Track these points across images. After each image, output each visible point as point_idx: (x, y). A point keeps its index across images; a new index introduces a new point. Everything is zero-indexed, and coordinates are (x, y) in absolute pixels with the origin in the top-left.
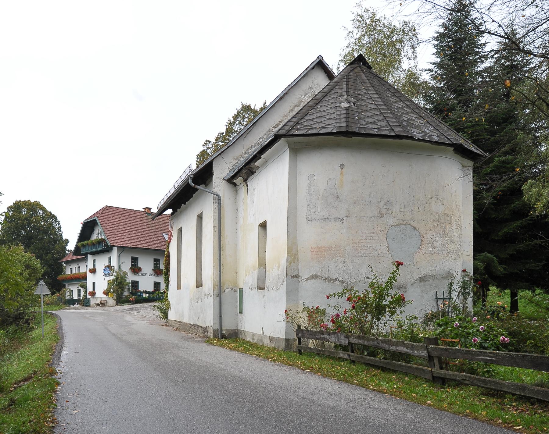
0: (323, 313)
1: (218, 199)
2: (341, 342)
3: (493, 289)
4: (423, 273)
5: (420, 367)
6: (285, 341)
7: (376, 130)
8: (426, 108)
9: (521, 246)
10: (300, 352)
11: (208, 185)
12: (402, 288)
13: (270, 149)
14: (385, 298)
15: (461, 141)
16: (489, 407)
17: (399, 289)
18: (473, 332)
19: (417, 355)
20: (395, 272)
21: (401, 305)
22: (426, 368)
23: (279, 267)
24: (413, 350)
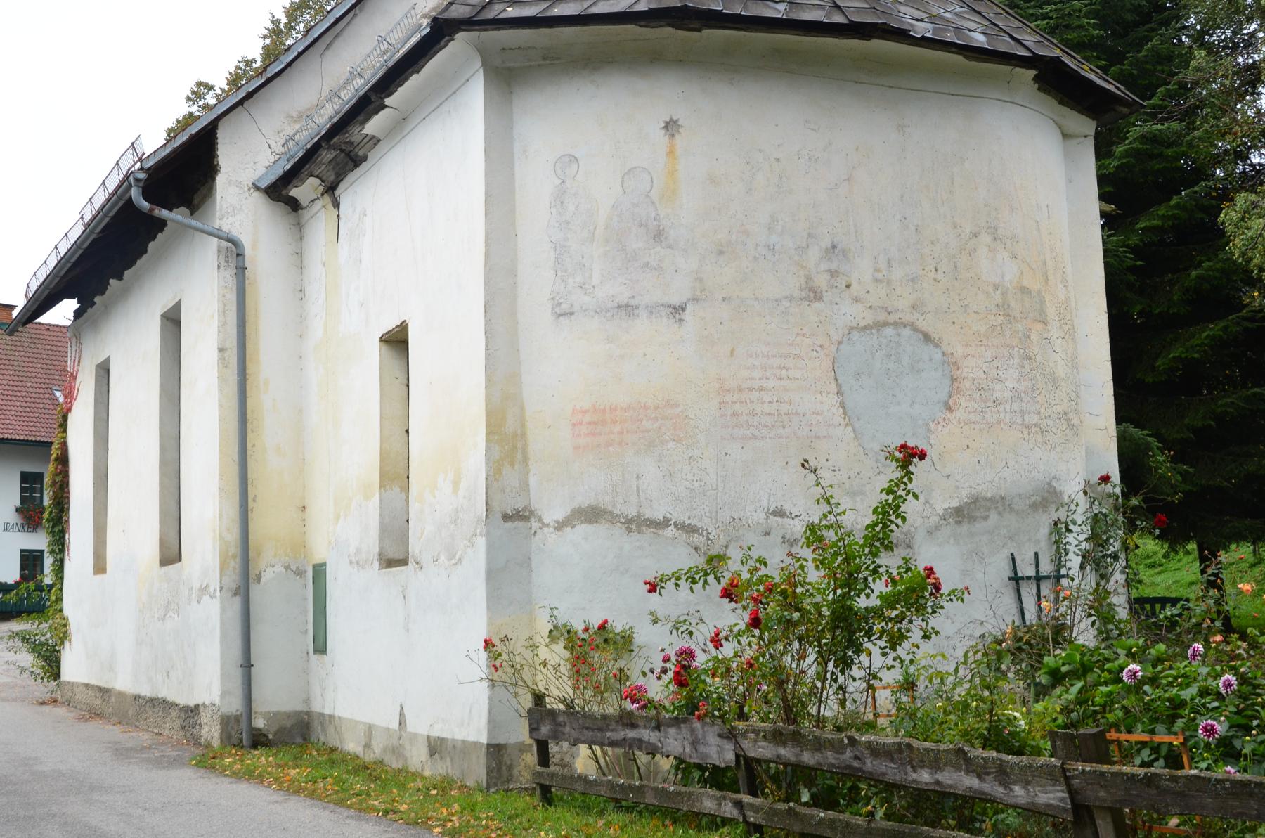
0: (624, 643)
1: (235, 252)
2: (707, 756)
4: (964, 493)
6: (488, 753)
9: (1229, 400)
10: (546, 795)
13: (418, 72)
23: (456, 484)
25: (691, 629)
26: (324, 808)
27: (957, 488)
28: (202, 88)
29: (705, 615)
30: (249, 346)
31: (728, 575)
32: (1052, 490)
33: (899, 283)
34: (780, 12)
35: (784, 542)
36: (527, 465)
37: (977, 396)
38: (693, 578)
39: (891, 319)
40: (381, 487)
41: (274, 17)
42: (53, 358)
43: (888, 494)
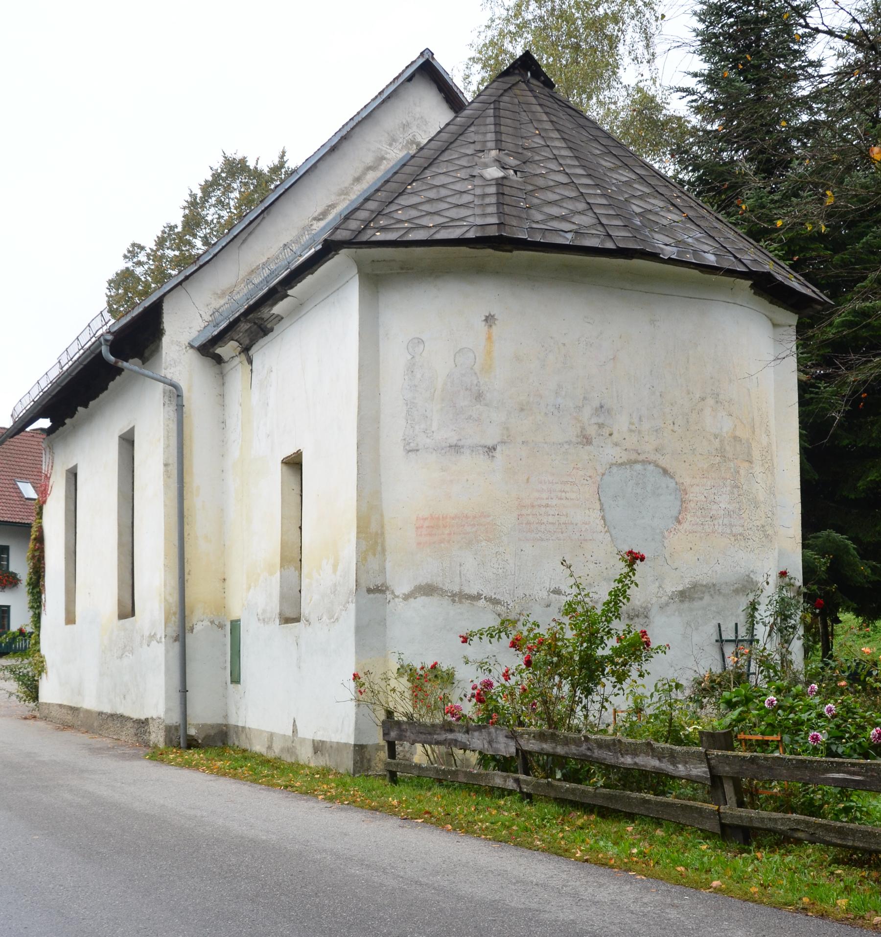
0: (448, 678)
2: (497, 750)
3: (847, 618)
4: (687, 581)
5: (692, 803)
6: (355, 750)
7: (570, 236)
8: (681, 180)
10: (393, 778)
11: (148, 360)
12: (638, 616)
13: (312, 274)
14: (602, 641)
15: (769, 267)
16: (852, 890)
17: (632, 619)
18: (808, 720)
19: (683, 774)
20: (625, 577)
21: (640, 657)
22: (705, 806)
24: (674, 764)
25: (490, 668)
26: (244, 784)
27: (682, 577)
28: (135, 249)
29: (499, 658)
30: (186, 462)
31: (514, 633)
32: (750, 580)
33: (646, 433)
34: (568, 239)
35: (560, 612)
36: (384, 555)
37: (699, 513)
38: (492, 634)
39: (640, 458)
40: (281, 567)
41: (192, 192)
42: (16, 456)
43: (618, 583)
